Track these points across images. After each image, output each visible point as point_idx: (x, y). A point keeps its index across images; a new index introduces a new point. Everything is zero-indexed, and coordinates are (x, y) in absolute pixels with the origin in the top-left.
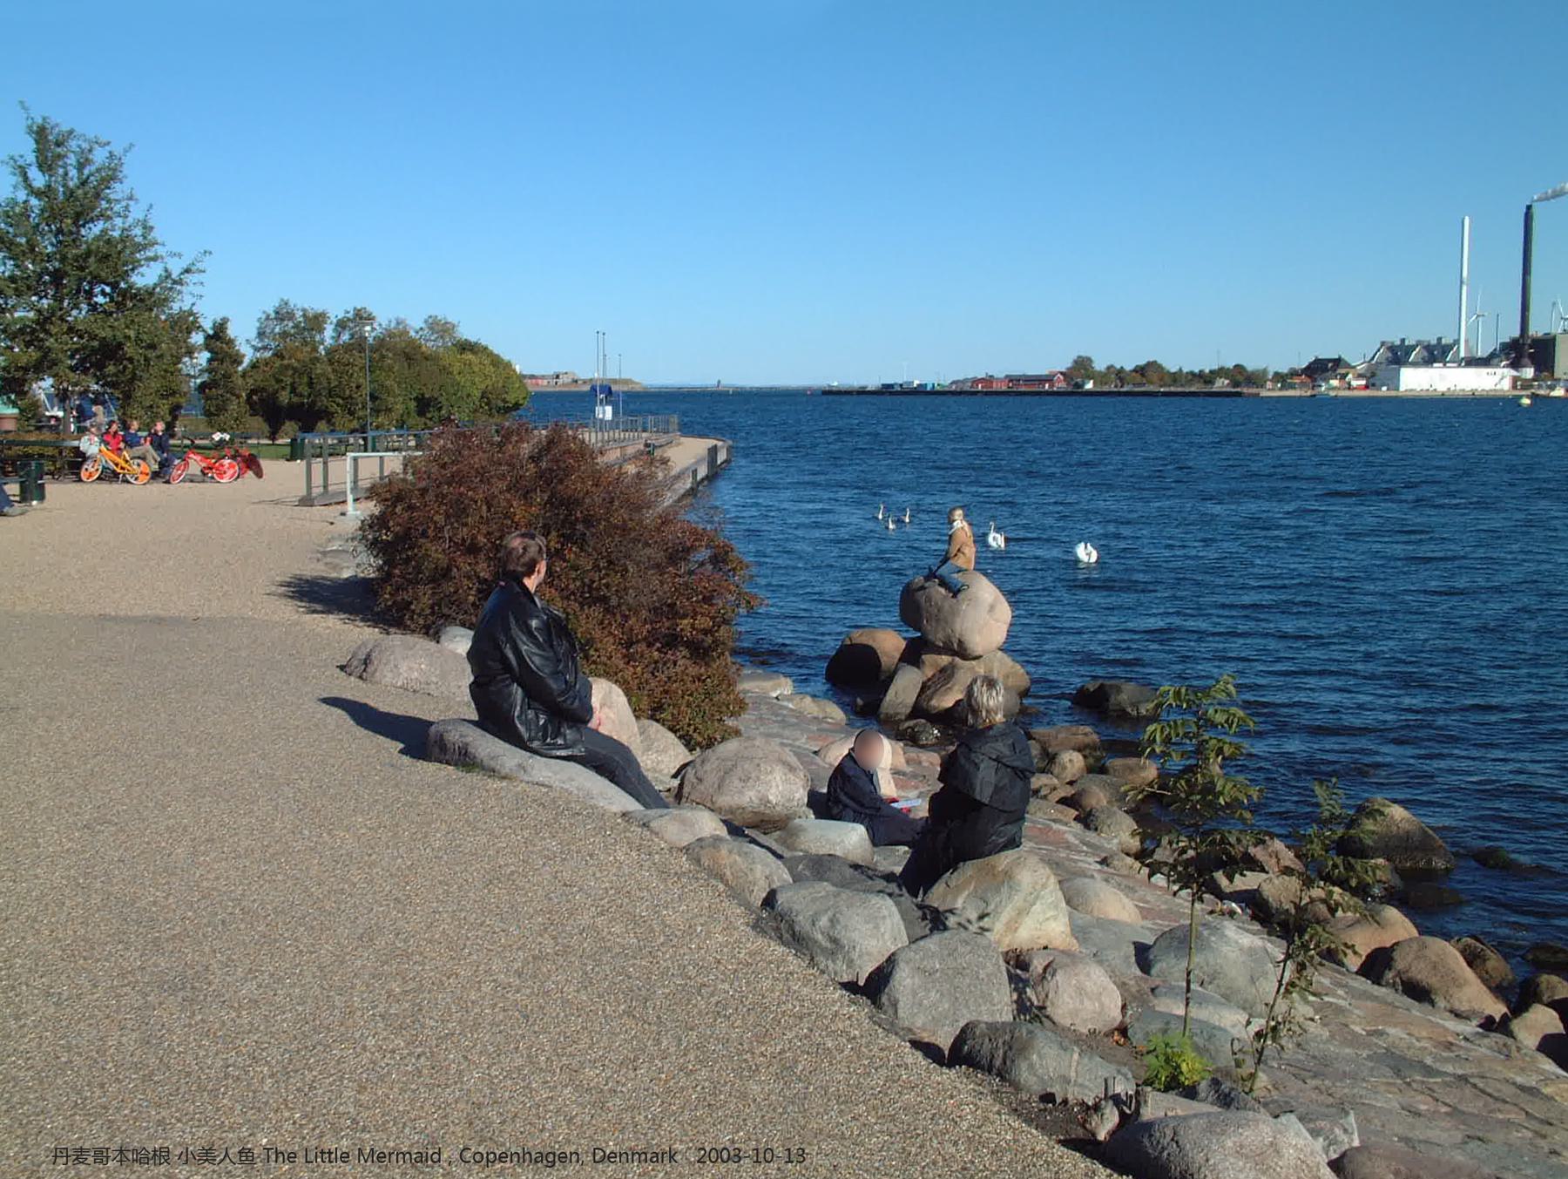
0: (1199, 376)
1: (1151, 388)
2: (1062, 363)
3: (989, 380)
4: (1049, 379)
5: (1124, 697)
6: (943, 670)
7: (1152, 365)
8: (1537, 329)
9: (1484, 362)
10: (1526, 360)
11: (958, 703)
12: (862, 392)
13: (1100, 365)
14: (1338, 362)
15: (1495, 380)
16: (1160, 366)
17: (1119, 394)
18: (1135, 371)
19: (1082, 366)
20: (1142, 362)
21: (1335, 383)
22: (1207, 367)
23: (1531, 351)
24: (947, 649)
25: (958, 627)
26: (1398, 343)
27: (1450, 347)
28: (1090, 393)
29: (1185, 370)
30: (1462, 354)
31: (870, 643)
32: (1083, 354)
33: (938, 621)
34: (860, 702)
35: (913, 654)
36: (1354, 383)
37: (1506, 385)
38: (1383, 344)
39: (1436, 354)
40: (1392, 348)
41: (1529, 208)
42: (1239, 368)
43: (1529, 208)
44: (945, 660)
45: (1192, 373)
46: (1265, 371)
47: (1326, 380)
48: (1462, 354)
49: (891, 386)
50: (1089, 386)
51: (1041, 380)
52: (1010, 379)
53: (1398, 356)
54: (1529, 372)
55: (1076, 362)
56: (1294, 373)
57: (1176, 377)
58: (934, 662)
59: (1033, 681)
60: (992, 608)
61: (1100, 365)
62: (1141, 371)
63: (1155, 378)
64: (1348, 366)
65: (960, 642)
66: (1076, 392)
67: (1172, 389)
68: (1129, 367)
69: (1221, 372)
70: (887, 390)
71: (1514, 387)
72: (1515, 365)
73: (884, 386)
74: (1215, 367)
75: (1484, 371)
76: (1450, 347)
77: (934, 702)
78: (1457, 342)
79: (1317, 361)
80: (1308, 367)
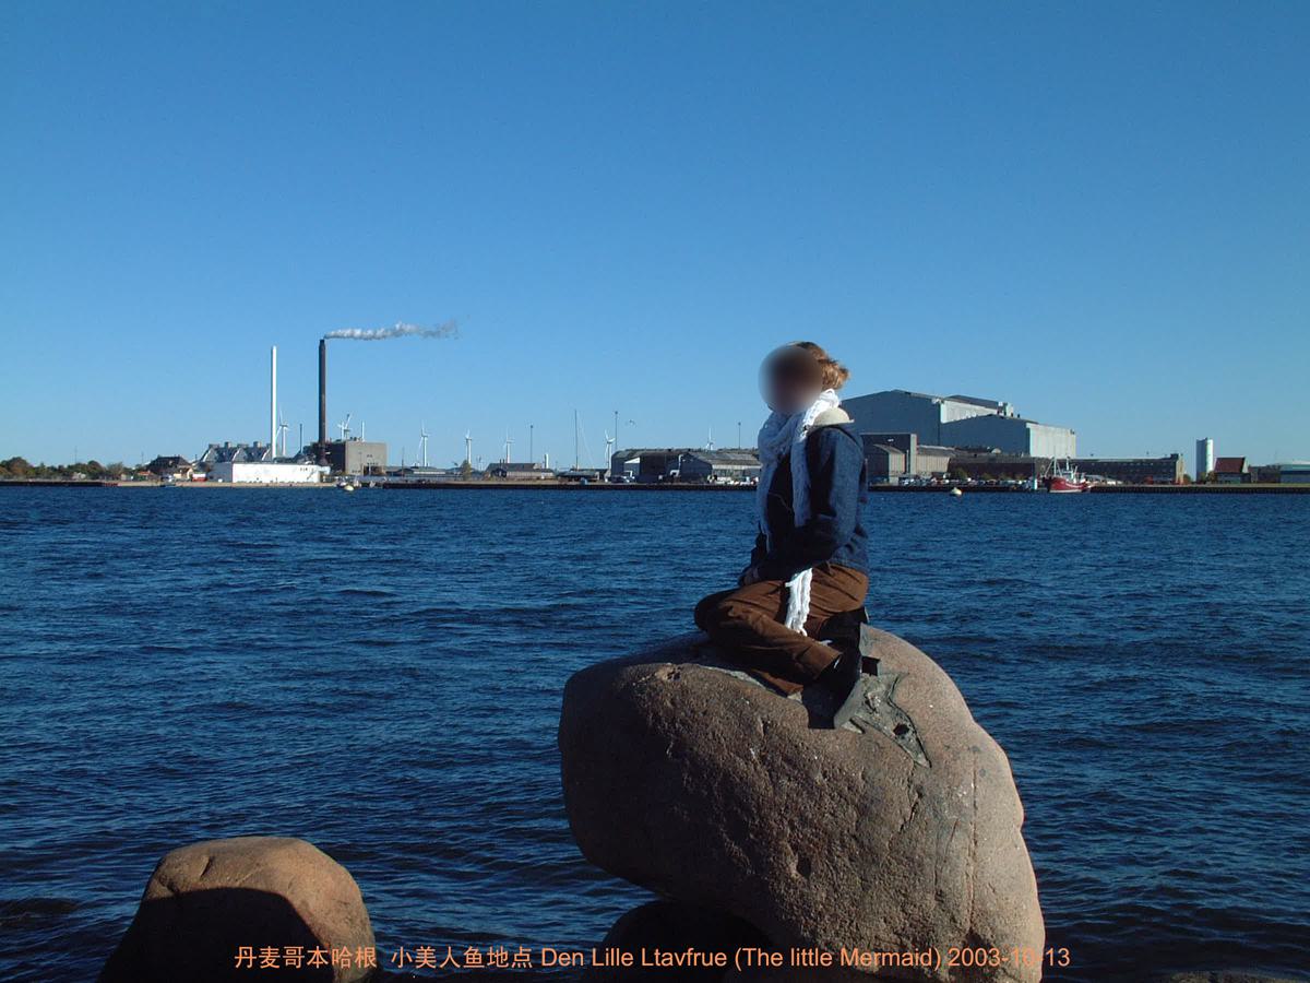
0: (60, 470)
1: (21, 479)
8: (331, 437)
9: (293, 461)
10: (324, 461)
14: (177, 460)
15: (306, 475)
16: (24, 462)
21: (178, 476)
22: (66, 461)
23: (329, 453)
29: (47, 465)
30: (274, 456)
31: (261, 886)
37: (315, 479)
38: (210, 446)
39: (254, 455)
40: (218, 450)
41: (322, 342)
43: (322, 342)
45: (53, 468)
47: (172, 473)
48: (274, 456)
53: (225, 455)
54: (327, 470)
56: (140, 469)
57: (38, 471)
63: (19, 470)
64: (186, 463)
67: (38, 480)
71: (322, 481)
72: (318, 462)
74: (73, 463)
75: (298, 467)
79: (160, 459)
80: (153, 463)
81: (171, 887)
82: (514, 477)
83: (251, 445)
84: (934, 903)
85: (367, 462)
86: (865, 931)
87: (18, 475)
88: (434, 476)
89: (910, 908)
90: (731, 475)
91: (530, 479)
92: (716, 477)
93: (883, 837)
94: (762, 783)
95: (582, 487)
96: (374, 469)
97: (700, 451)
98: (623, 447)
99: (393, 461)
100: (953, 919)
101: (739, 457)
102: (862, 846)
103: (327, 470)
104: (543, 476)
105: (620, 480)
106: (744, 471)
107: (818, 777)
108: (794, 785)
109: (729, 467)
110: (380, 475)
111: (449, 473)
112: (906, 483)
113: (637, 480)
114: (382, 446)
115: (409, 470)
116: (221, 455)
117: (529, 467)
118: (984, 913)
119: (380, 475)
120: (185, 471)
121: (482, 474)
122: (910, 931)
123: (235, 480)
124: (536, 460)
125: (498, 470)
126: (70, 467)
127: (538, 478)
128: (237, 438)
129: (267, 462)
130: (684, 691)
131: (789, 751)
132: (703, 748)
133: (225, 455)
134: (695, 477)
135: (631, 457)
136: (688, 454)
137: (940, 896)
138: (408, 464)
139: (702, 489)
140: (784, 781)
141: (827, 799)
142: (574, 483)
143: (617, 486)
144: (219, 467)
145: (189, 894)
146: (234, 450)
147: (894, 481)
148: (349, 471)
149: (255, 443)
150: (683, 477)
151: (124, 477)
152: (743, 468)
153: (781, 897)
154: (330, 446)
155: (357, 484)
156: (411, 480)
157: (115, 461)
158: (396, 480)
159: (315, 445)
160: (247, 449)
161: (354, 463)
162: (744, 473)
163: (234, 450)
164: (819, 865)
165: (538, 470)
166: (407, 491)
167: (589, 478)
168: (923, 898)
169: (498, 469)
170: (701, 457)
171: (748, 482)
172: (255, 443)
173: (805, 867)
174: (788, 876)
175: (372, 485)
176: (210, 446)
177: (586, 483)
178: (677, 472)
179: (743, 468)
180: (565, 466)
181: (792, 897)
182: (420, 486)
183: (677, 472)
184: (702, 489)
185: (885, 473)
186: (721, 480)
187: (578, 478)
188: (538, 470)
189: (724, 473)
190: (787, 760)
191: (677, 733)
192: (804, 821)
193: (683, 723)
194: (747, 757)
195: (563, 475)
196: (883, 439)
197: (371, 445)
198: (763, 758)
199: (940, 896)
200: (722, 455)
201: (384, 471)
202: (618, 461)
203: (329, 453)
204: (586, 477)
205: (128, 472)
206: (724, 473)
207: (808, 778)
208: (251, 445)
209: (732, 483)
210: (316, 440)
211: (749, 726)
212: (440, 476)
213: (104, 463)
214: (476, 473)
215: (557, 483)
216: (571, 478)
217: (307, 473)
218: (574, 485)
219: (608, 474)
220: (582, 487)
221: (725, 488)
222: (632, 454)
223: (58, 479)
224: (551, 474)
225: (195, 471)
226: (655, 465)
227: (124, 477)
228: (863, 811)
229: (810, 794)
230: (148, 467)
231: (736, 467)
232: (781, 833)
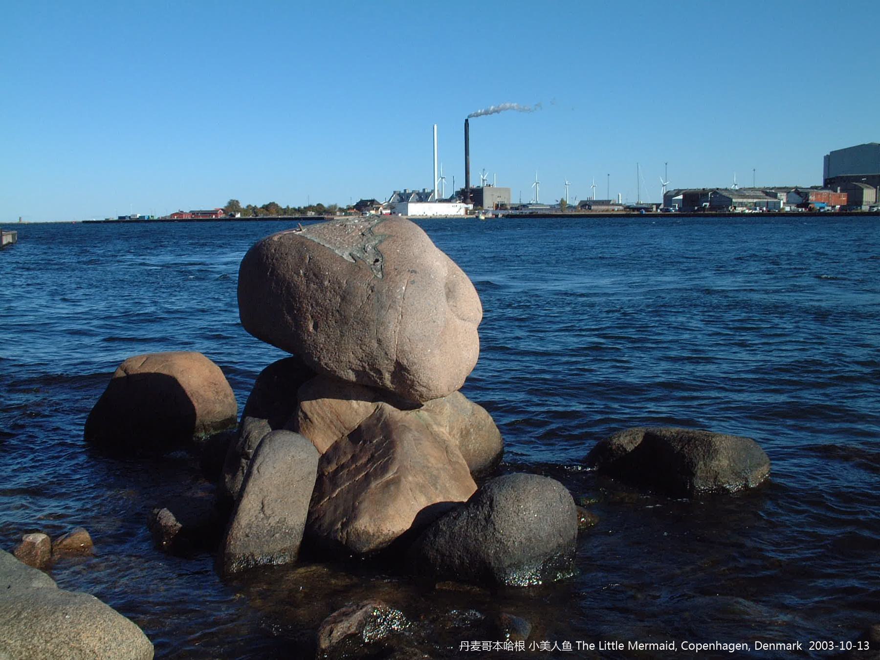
0: (299, 210)
1: (274, 216)
2: (223, 204)
3: (181, 213)
4: (215, 212)
5: (722, 462)
6: (357, 435)
7: (272, 205)
8: (473, 184)
9: (449, 201)
10: (469, 200)
11: (431, 518)
12: (107, 222)
13: (243, 205)
14: (373, 202)
15: (457, 210)
16: (277, 205)
17: (255, 219)
18: (263, 208)
19: (233, 205)
20: (267, 203)
21: (373, 212)
22: (303, 204)
23: (472, 195)
24: (368, 387)
25: (392, 332)
26: (402, 192)
27: (429, 194)
28: (238, 219)
29: (291, 207)
30: (436, 197)
31: (165, 372)
32: (234, 198)
33: (343, 321)
34: (168, 518)
35: (280, 397)
36: (384, 212)
37: (462, 213)
38: (395, 192)
39: (423, 197)
40: (400, 195)
41: (467, 121)
42: (320, 206)
43: (467, 121)
44: (359, 410)
45: (294, 209)
46: (335, 207)
47: (369, 211)
48: (436, 197)
49: (124, 218)
50: (238, 216)
51: (211, 213)
52: (193, 213)
53: (404, 198)
54: (471, 206)
55: (230, 203)
56: (349, 208)
57: (285, 211)
58: (335, 416)
59: (772, 475)
60: (450, 292)
61: (243, 205)
62: (266, 208)
63: (273, 211)
64: (379, 204)
65: (401, 371)
66: (232, 219)
67: (285, 216)
68: (259, 206)
69: (310, 208)
70: (122, 220)
71: (466, 213)
72: (464, 201)
73: (120, 218)
74: (307, 205)
75: (450, 205)
76: (429, 194)
77: (364, 524)
78: (433, 191)
79: (362, 201)
80: (358, 204)
81: (125, 371)
82: (597, 209)
83: (421, 191)
84: (376, 345)
85: (498, 201)
86: (342, 358)
87: (272, 213)
88: (542, 209)
89: (364, 347)
90: (746, 206)
91: (607, 211)
92: (735, 207)
93: (351, 311)
94: (303, 288)
95: (641, 216)
96: (502, 205)
97: (726, 190)
98: (672, 188)
99: (514, 200)
100: (386, 353)
101: (752, 193)
102: (341, 315)
103: (471, 206)
104: (616, 208)
105: (667, 210)
106: (756, 203)
107: (326, 283)
108: (315, 286)
109: (745, 200)
110: (506, 209)
111: (552, 207)
112: (875, 209)
113: (680, 209)
114: (507, 190)
115: (524, 206)
116: (402, 198)
117: (607, 203)
118: (403, 351)
119: (506, 209)
120: (377, 209)
121: (575, 208)
122: (365, 359)
123: (409, 214)
124: (612, 197)
125: (586, 205)
126: (305, 208)
127: (613, 210)
128: (413, 186)
129: (431, 202)
130: (281, 244)
131: (316, 271)
132: (281, 271)
133: (404, 198)
134: (720, 207)
135: (677, 194)
136: (715, 192)
137: (379, 341)
138: (525, 202)
139: (725, 215)
140: (312, 285)
141: (328, 294)
142: (636, 213)
143: (666, 214)
144: (400, 206)
145: (134, 375)
146: (410, 194)
147: (865, 208)
148: (485, 206)
149: (424, 190)
150: (712, 208)
151: (338, 213)
152: (755, 201)
153: (305, 341)
154: (473, 191)
155: (490, 215)
156: (526, 212)
157: (333, 203)
158: (517, 212)
159: (463, 190)
160: (418, 194)
161: (489, 201)
162: (755, 204)
163: (410, 194)
164: (322, 325)
165: (613, 205)
166: (521, 218)
167: (646, 209)
168: (370, 342)
169: (584, 205)
170: (725, 194)
171: (758, 211)
172: (424, 190)
173: (316, 327)
174: (308, 331)
175: (500, 216)
176: (395, 192)
177: (644, 212)
178: (708, 204)
179: (755, 201)
180: (632, 201)
181: (309, 342)
182: (533, 216)
183: (708, 204)
184: (725, 215)
185: (860, 203)
186: (739, 210)
187: (638, 209)
188: (613, 205)
189: (742, 204)
190: (315, 275)
191: (273, 265)
192: (318, 304)
193: (277, 259)
194: (298, 274)
195: (628, 208)
196: (858, 179)
197: (499, 189)
198: (305, 274)
199: (379, 341)
200: (741, 193)
201: (509, 207)
202: (668, 198)
203: (472, 195)
204: (644, 208)
205: (341, 210)
206: (742, 204)
207: (322, 283)
208: (421, 191)
209: (747, 211)
210: (464, 186)
211: (302, 259)
212: (546, 209)
213: (326, 205)
214: (570, 207)
215: (624, 213)
216: (634, 209)
217: (457, 209)
218: (637, 215)
219: (662, 207)
220: (641, 216)
221: (742, 215)
222: (678, 192)
223: (297, 216)
224: (621, 208)
225: (384, 209)
226: (693, 199)
227: (338, 213)
228: (343, 299)
229: (322, 291)
230: (354, 207)
231: (750, 200)
232: (307, 310)
